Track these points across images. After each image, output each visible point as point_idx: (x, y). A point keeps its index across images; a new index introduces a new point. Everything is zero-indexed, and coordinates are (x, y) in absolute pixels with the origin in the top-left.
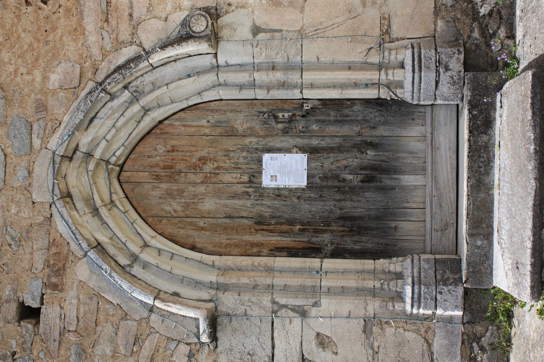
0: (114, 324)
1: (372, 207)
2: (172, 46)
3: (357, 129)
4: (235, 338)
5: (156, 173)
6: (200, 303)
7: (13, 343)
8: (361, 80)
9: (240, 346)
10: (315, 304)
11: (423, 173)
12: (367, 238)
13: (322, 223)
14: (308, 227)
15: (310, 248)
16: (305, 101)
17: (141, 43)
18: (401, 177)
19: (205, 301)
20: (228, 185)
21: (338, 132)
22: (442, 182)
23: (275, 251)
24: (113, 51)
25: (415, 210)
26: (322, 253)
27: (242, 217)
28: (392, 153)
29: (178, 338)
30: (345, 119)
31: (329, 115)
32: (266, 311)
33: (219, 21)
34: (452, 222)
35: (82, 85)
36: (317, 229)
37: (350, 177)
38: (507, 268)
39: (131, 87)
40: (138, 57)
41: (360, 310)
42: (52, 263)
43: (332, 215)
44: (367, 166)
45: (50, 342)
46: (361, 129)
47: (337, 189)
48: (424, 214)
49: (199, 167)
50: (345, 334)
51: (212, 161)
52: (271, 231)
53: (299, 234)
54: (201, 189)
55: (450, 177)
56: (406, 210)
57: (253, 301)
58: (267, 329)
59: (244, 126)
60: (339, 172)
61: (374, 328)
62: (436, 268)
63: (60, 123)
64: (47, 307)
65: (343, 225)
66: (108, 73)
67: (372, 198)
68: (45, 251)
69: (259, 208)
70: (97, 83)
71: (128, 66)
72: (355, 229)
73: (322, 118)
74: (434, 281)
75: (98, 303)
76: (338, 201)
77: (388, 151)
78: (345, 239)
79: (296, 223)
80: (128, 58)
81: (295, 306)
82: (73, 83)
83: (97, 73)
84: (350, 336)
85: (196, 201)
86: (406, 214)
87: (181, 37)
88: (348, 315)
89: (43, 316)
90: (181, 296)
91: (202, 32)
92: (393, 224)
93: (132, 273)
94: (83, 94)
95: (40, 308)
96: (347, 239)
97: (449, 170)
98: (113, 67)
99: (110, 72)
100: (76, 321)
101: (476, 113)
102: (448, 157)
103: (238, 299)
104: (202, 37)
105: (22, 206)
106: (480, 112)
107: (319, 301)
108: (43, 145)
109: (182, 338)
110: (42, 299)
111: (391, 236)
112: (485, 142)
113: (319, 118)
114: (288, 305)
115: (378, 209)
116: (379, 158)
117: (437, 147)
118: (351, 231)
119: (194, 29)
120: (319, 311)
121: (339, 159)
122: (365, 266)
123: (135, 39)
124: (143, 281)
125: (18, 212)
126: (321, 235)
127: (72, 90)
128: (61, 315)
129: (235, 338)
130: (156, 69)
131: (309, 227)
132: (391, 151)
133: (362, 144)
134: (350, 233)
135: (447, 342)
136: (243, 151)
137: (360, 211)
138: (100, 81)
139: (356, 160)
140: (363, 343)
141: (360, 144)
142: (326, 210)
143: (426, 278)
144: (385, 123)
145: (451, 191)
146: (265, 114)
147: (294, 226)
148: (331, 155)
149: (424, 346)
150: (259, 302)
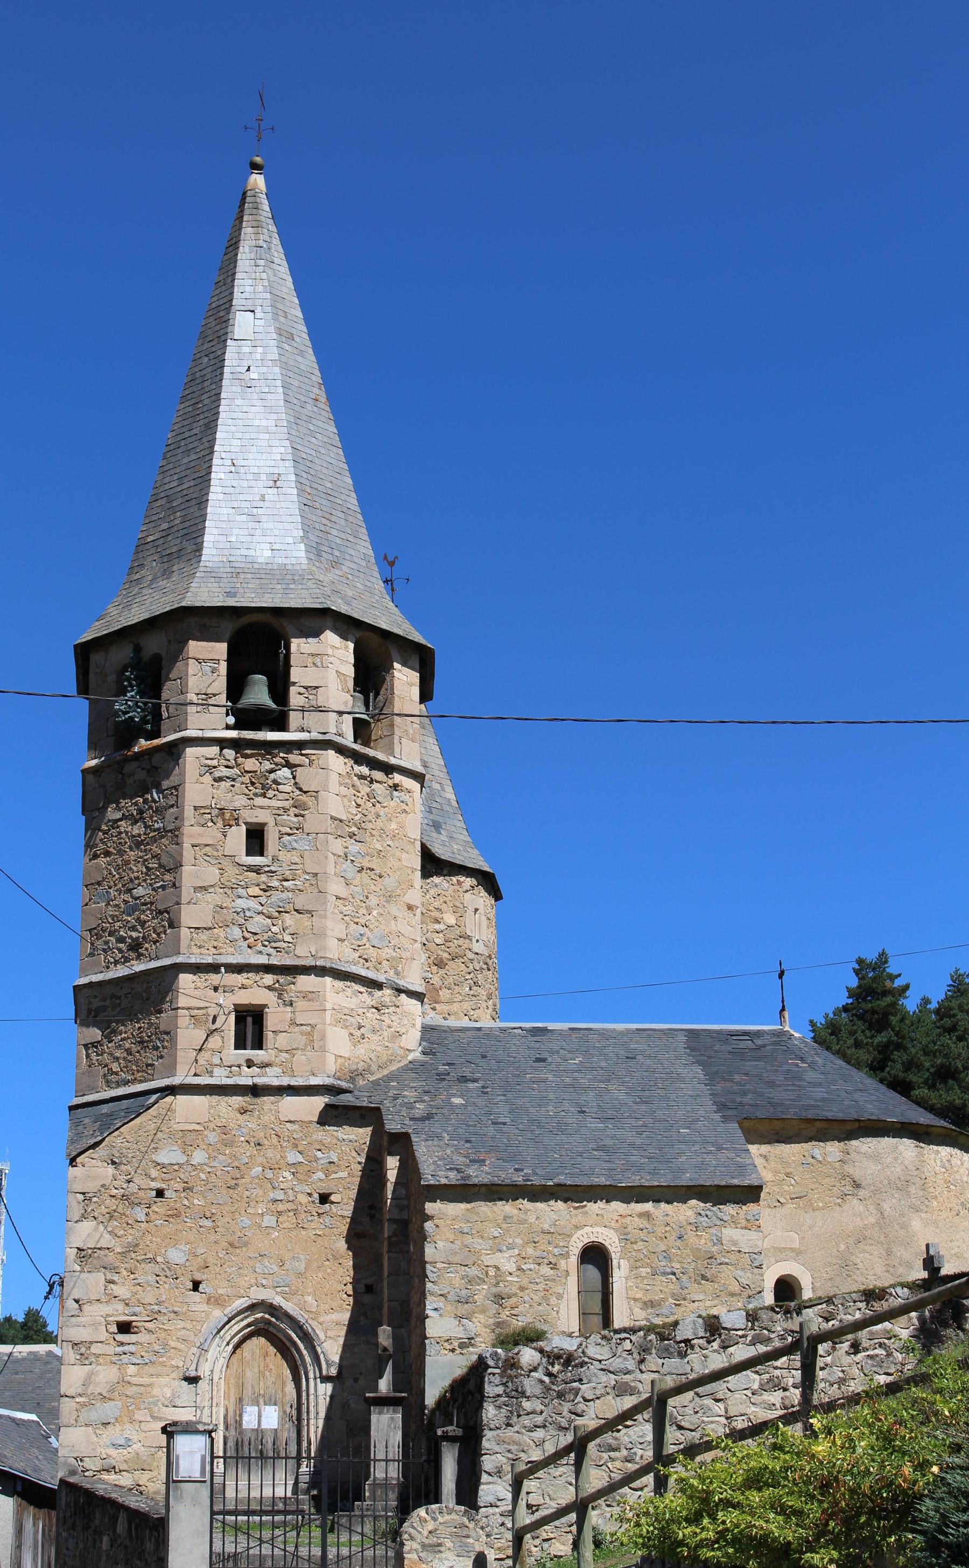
54: (257, 1371)
69: (247, 1399)
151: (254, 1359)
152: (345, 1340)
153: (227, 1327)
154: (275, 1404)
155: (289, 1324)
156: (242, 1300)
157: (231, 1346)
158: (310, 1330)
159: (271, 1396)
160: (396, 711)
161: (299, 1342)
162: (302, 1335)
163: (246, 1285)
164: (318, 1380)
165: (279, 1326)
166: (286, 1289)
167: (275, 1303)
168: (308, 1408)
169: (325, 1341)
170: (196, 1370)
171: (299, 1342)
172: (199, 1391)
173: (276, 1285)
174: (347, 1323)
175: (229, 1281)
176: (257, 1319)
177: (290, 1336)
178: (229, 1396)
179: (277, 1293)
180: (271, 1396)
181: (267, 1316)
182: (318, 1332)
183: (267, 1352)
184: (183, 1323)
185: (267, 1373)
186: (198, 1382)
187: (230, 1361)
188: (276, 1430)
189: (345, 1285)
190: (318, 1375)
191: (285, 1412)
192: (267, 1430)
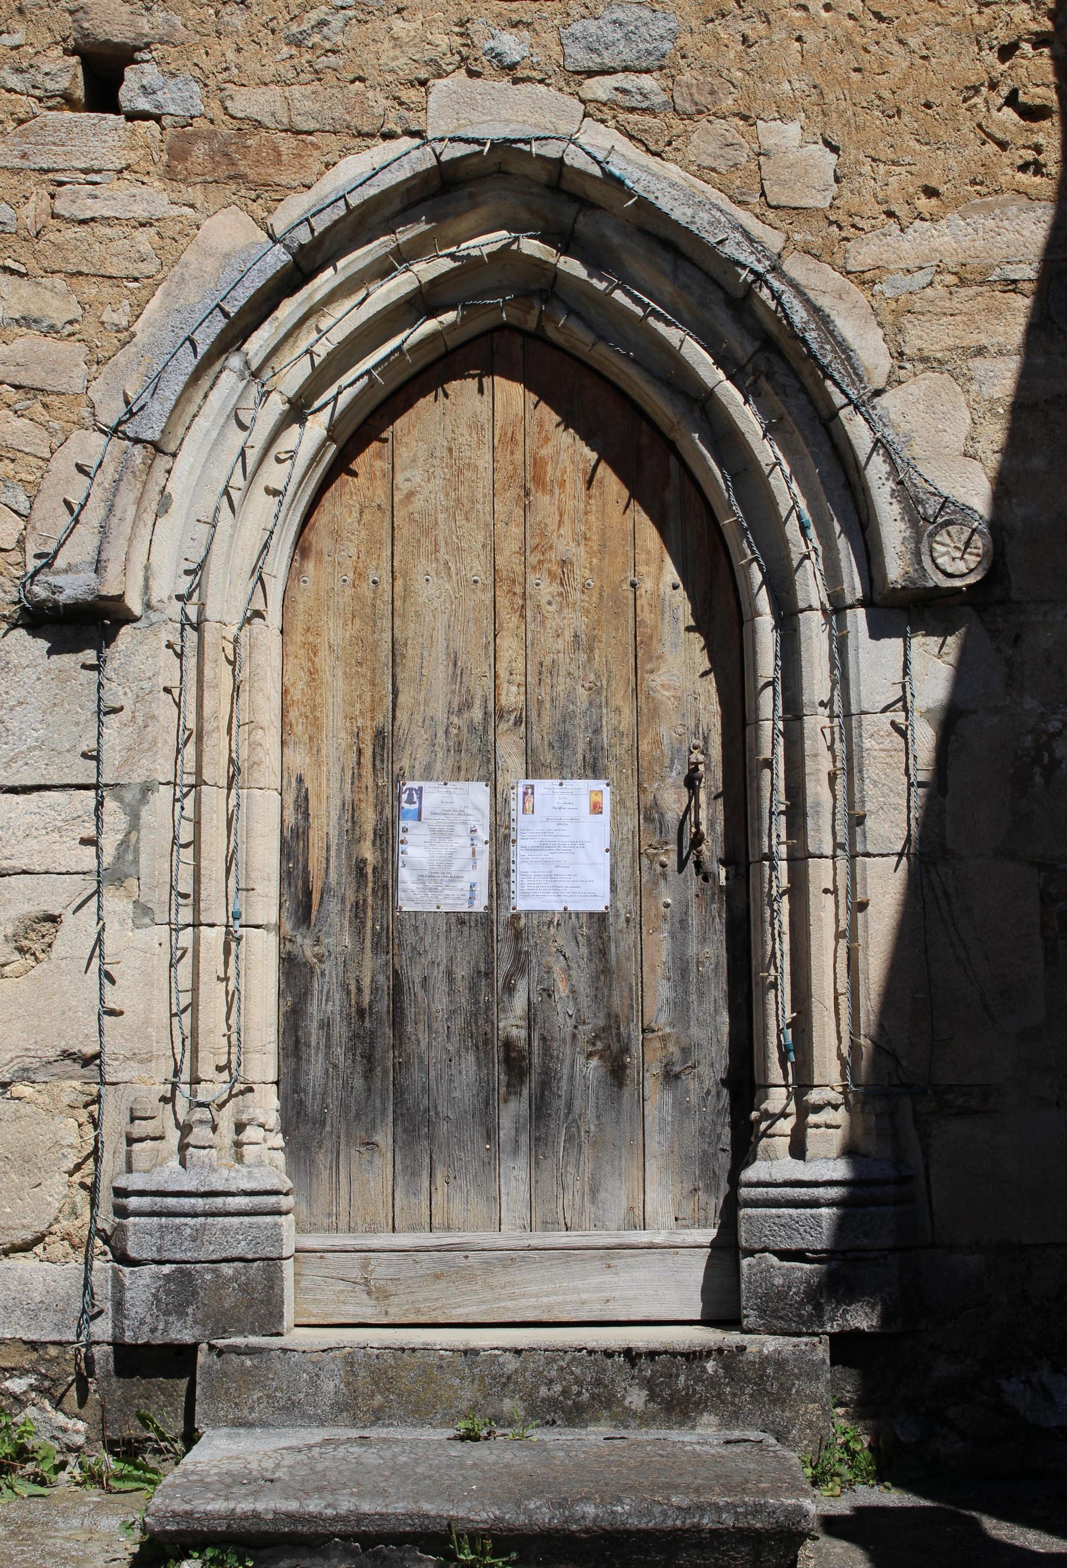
0: (77, 327)
1: (432, 1073)
2: (889, 474)
3: (662, 1020)
4: (39, 679)
5: (520, 437)
6: (140, 575)
7: (16, 36)
8: (804, 1031)
9: (15, 695)
10: (143, 910)
11: (537, 1218)
12: (342, 1058)
13: (382, 926)
14: (370, 885)
15: (308, 894)
16: (742, 870)
17: (900, 383)
18: (522, 1161)
19: (147, 587)
20: (492, 648)
21: (653, 970)
22: (508, 1278)
23: (299, 791)
24: (873, 303)
25: (425, 1203)
26: (293, 929)
27: (395, 693)
28: (592, 1128)
29: (36, 515)
30: (693, 988)
31: (703, 940)
32: (120, 766)
33: (968, 609)
34: (392, 1310)
35: (771, 215)
36: (365, 913)
37: (519, 1003)
38: (250, 1458)
39: (768, 359)
40: (857, 375)
41: (127, 1040)
42: (249, 142)
43: (407, 952)
44: (552, 1056)
45: (20, 144)
46: (664, 1039)
47: (483, 969)
48: (413, 1228)
49: (540, 562)
50: (56, 998)
51: (559, 599)
52: (357, 777)
53: (349, 857)
54: (477, 568)
55: (525, 1302)
56: (425, 1174)
57: (149, 729)
58: (66, 770)
59: (666, 693)
60: (535, 974)
61: (76, 1084)
62: (254, 1260)
63: (655, 154)
64: (121, 132)
65: (377, 989)
66: (806, 291)
67: (460, 1073)
68: (285, 121)
69: (421, 737)
70: (779, 256)
71: (828, 347)
72: (367, 1024)
73: (694, 922)
74: (214, 1257)
75: (136, 280)
76: (450, 974)
77: (598, 1117)
78: (337, 996)
79: (382, 850)
80: (853, 347)
81: (137, 851)
82: (776, 189)
83: (808, 257)
84: (49, 1012)
85: (443, 555)
86: (415, 1174)
87: (918, 501)
88: (138, 1114)
89: (96, 121)
90: (159, 520)
91: (933, 560)
92: (384, 1138)
93: (224, 375)
94: (744, 217)
95: (116, 109)
96: (337, 1002)
97: (545, 1300)
98: (824, 302)
99: (811, 295)
100: (82, 217)
101: (710, 1371)
102: (584, 1296)
103: (153, 686)
104: (920, 562)
105: (413, 50)
106: (713, 1382)
107: (152, 920)
108: (593, 105)
109: (38, 524)
110: (145, 116)
111: (348, 1134)
112: (624, 1398)
113: (693, 910)
114: (139, 831)
115: (427, 1090)
116: (578, 1094)
117: (613, 1263)
118: (361, 1013)
119: (940, 538)
120: (122, 923)
121: (573, 973)
122: (258, 1055)
123: (908, 365)
124: (200, 407)
125: (396, 39)
126: (346, 923)
127: (757, 187)
128: (99, 171)
129: (39, 679)
130: (822, 429)
131: (369, 890)
132: (600, 1126)
133: (619, 1041)
134: (353, 1009)
135: (38, 1299)
136: (590, 689)
137: (421, 1036)
138: (784, 268)
139: (571, 1022)
140: (33, 1053)
141: (619, 1035)
142: (422, 939)
143: (224, 1230)
144: (682, 1109)
145: (484, 1307)
146: (702, 753)
147: (374, 844)
148: (584, 950)
149: (24, 1232)
150: (146, 746)
151: (459, 508)
152: (1026, 377)
153: (289, 310)
154: (593, 769)
155: (668, 288)
156: (381, 152)
157: (317, 426)
158: (799, 315)
159: (567, 717)
160: (815, 1083)
161: (730, 394)
162: (743, 348)
163: (402, 64)
164: (858, 618)
165: (604, 301)
166: (647, 82)
167: (576, 159)
168: (796, 790)
169: (895, 381)
170: (98, 566)
171: (730, 394)
172: (114, 694)
173: (582, 58)
174: (1027, 272)
175: (296, 42)
176: (471, 265)
177: (673, 356)
178: (315, 723)
179: (592, 110)
180: (567, 717)
181: (531, 247)
182: (846, 327)
183: (539, 464)
184: (25, 288)
185: (546, 590)
186: (109, 637)
187: (321, 518)
188: (599, 919)
189: (1007, 52)
190: (853, 585)
191: (651, 814)
192: (547, 920)
